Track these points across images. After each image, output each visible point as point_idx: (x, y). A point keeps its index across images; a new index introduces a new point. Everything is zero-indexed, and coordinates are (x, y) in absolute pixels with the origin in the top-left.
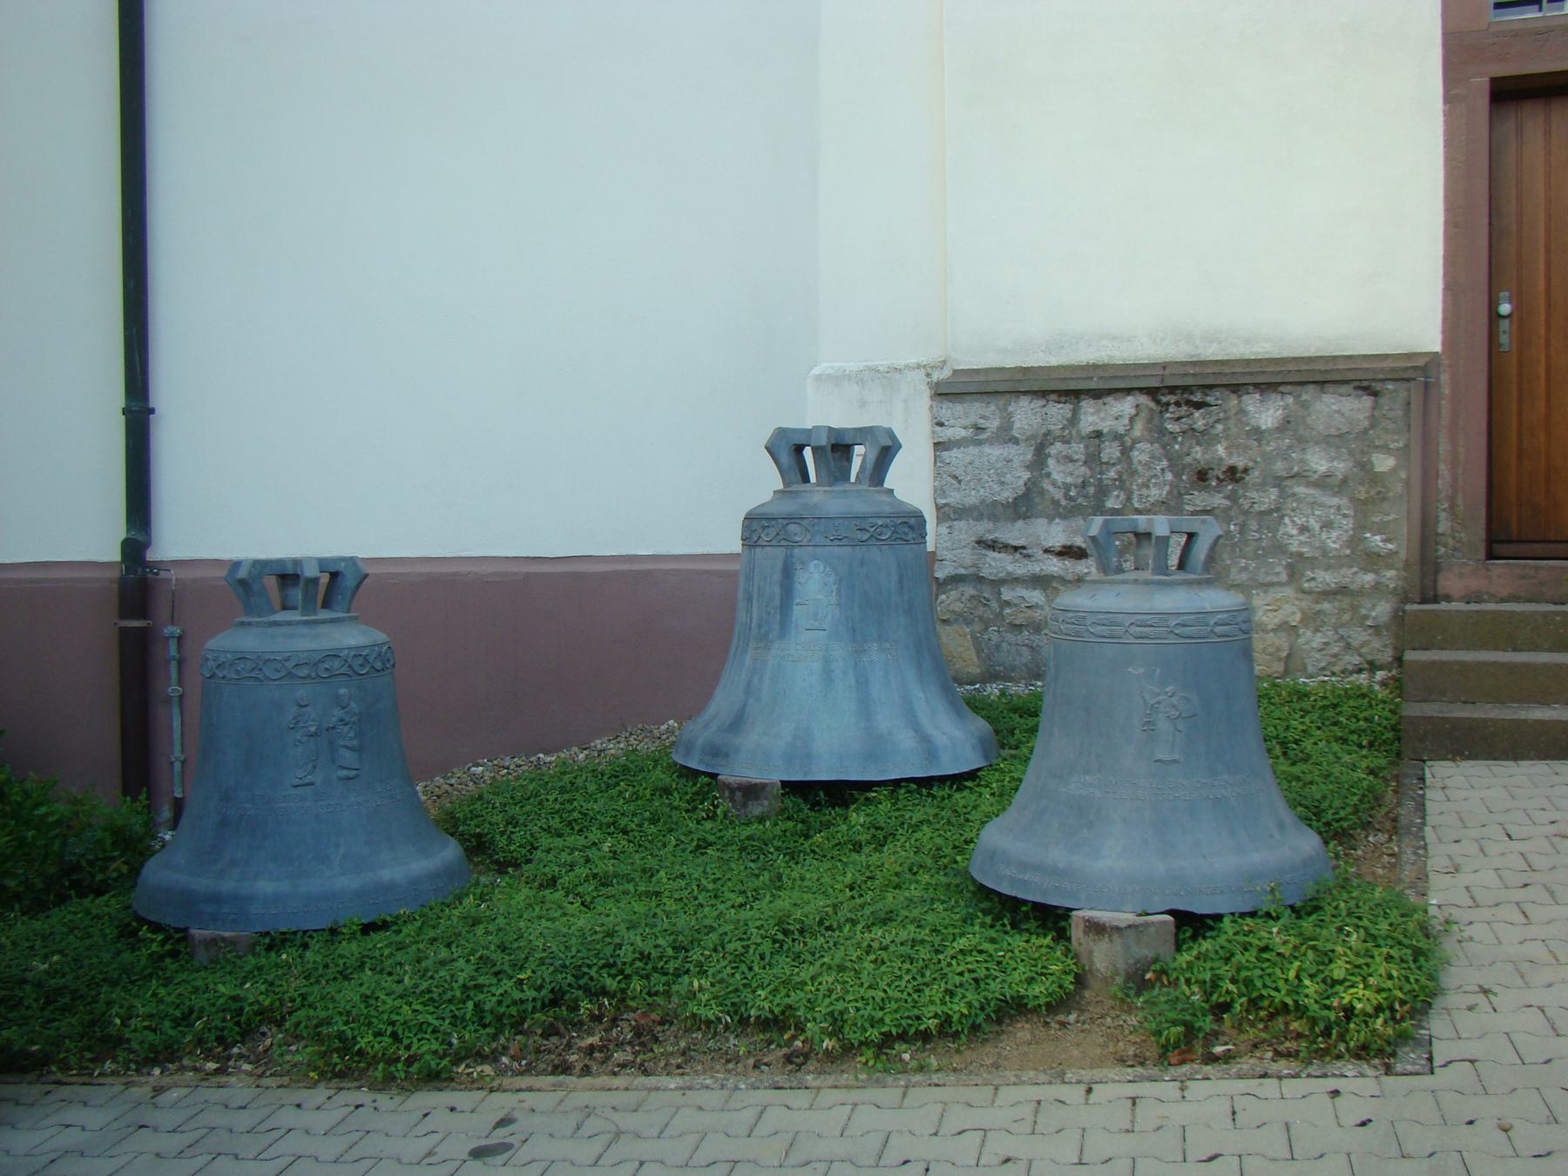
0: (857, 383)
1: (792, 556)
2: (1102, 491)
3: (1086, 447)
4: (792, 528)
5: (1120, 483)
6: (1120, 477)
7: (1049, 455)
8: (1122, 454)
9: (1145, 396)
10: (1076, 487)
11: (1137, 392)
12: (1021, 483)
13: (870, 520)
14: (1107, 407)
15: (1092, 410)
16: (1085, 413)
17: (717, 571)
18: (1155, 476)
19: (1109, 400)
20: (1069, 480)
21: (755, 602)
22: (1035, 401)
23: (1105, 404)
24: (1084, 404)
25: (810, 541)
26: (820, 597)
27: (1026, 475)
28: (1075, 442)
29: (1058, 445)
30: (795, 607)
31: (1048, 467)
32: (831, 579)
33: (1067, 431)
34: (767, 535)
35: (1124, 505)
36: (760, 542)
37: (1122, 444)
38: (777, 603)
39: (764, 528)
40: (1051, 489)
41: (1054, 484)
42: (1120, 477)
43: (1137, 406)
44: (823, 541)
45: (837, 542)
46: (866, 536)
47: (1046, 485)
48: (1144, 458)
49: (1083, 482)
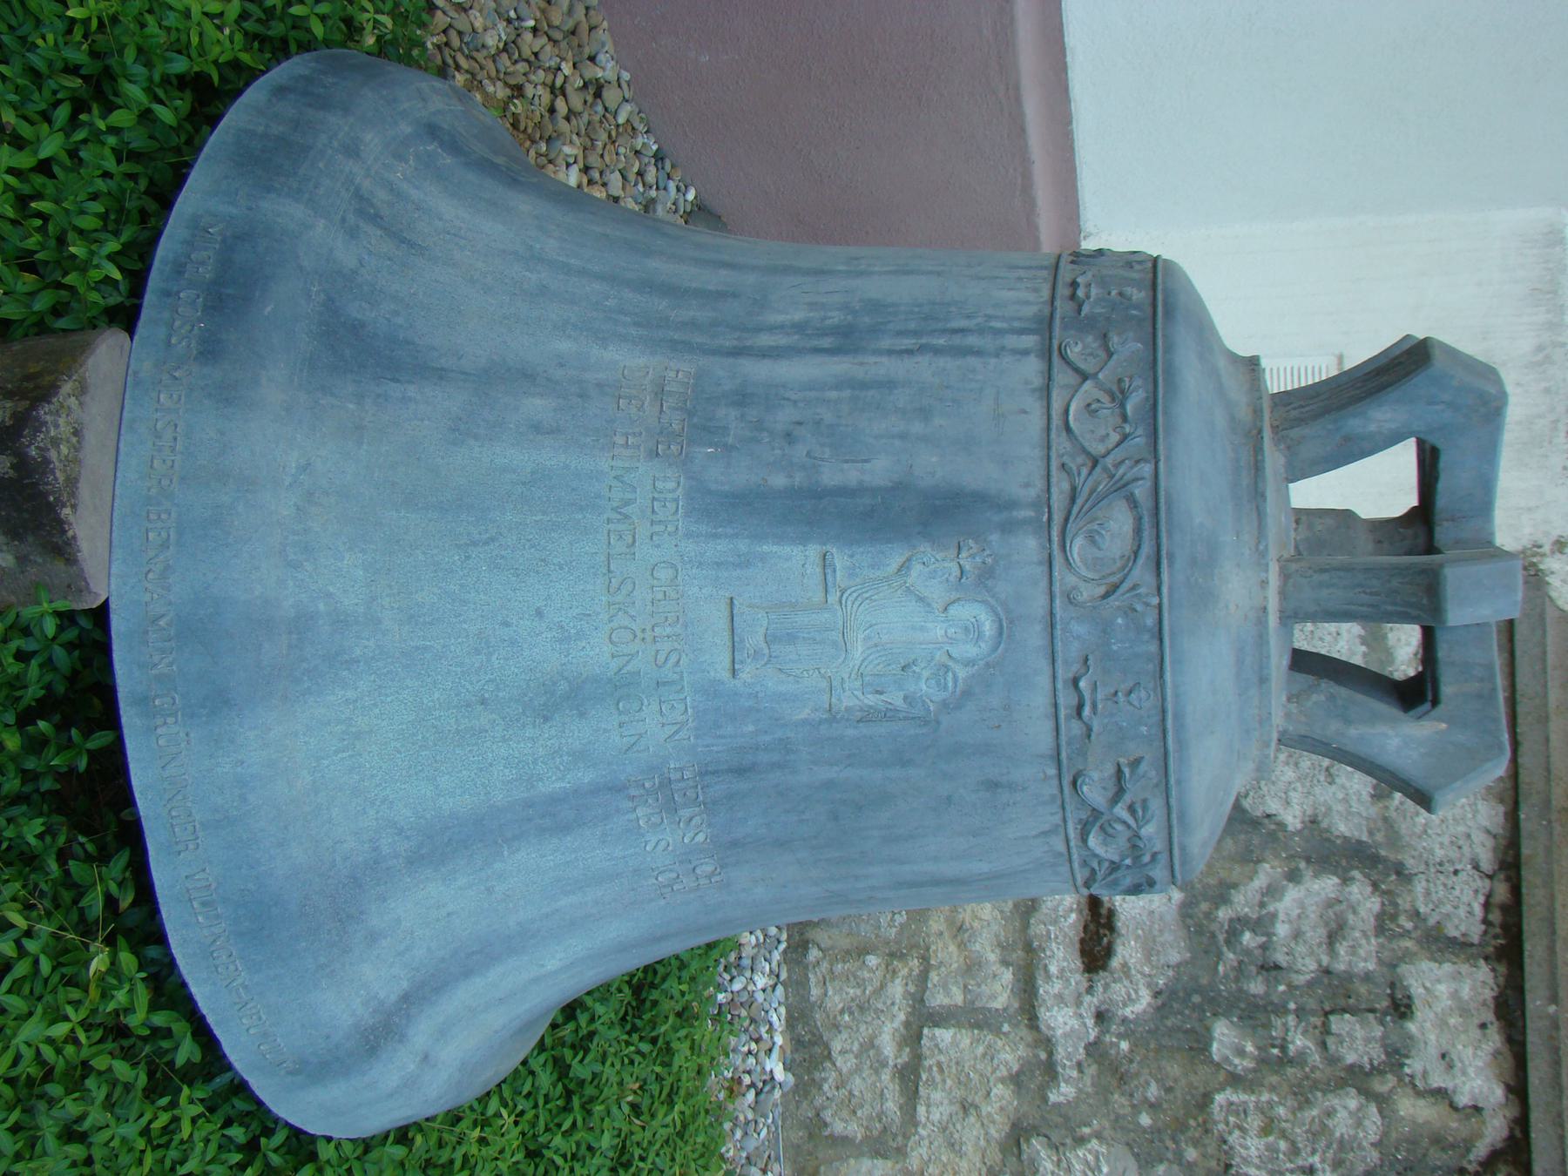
0: (1540, 348)
1: (1008, 528)
2: (1254, 1014)
3: (1367, 977)
4: (1119, 523)
5: (1277, 1061)
6: (1291, 1062)
7: (1346, 881)
8: (1351, 1068)
9: (1505, 1133)
10: (1264, 947)
11: (1513, 1112)
12: (1273, 806)
13: (1156, 805)
14: (1476, 1033)
15: (1466, 992)
16: (1457, 976)
17: (1012, 20)
18: (1295, 1151)
19: (1495, 1039)
20: (1282, 930)
21: (840, 366)
22: (1490, 843)
23: (1483, 1026)
24: (1483, 972)
25: (1070, 600)
26: (858, 652)
27: (1292, 819)
28: (1382, 946)
29: (1373, 904)
30: (813, 551)
31: (1316, 876)
32: (924, 687)
33: (1409, 925)
34: (1090, 409)
35: (1218, 1066)
36: (1062, 376)
37: (1377, 1071)
38: (830, 476)
39: (1119, 396)
40: (1260, 882)
41: (1272, 891)
42: (1291, 1062)
43: (1477, 1109)
44: (1070, 651)
45: (1067, 700)
46: (1095, 792)
47: (1267, 872)
48: (1341, 1125)
49: (1277, 967)
